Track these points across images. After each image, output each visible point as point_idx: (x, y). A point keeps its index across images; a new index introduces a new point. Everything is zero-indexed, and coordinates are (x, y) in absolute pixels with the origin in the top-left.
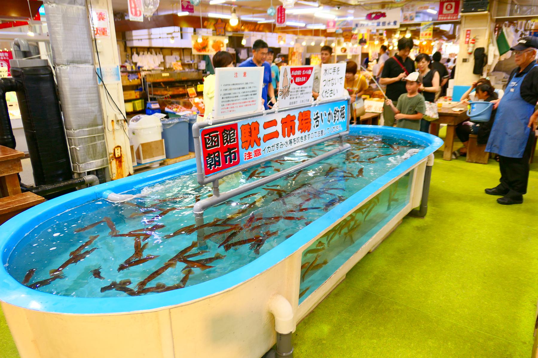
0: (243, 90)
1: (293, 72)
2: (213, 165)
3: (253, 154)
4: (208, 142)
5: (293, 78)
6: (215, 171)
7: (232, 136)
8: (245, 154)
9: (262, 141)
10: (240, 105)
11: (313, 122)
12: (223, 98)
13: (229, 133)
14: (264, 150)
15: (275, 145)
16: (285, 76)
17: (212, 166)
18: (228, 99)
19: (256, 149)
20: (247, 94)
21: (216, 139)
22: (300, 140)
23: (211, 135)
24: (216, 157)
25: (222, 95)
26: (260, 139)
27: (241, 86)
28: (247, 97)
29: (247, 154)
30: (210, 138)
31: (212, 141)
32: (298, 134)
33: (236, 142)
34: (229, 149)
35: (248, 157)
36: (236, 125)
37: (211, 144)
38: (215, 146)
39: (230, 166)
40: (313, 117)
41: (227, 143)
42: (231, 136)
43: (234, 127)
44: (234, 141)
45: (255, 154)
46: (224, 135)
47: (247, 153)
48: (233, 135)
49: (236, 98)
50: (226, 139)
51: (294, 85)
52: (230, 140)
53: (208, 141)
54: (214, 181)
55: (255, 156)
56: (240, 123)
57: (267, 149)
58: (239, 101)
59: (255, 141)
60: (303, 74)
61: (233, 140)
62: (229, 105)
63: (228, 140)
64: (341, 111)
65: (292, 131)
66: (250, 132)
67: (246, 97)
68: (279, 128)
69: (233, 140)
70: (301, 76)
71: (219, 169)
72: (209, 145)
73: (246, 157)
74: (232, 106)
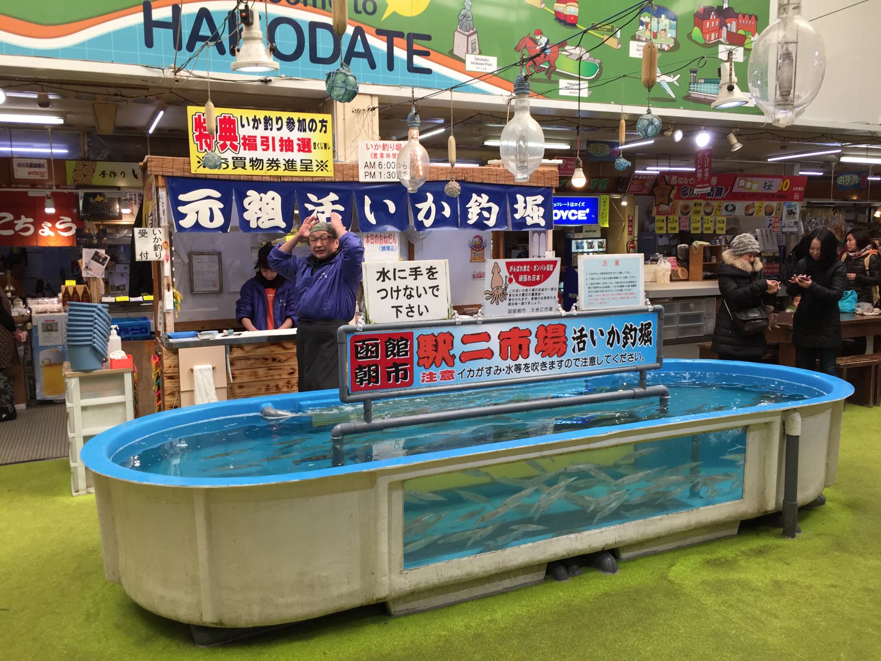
0: (616, 280)
1: (511, 268)
2: (365, 380)
3: (439, 377)
4: (361, 350)
5: (512, 276)
6: (367, 388)
7: (402, 348)
8: (424, 374)
9: (457, 360)
10: (614, 297)
11: (572, 343)
12: (589, 288)
13: (398, 343)
14: (461, 373)
15: (484, 369)
16: (496, 273)
17: (364, 382)
18: (596, 289)
19: (445, 370)
20: (622, 284)
21: (374, 348)
22: (539, 368)
23: (366, 343)
24: (372, 371)
25: (588, 284)
26: (454, 357)
27: (613, 276)
28: (622, 288)
29: (427, 375)
30: (365, 346)
31: (367, 350)
32: (534, 358)
33: (409, 356)
34: (396, 365)
35: (427, 378)
36: (412, 334)
37: (364, 353)
38: (374, 357)
39: (394, 386)
40: (570, 334)
41: (392, 356)
42: (401, 347)
43: (408, 337)
44: (406, 354)
45: (442, 376)
46: (389, 345)
47: (427, 373)
48: (404, 346)
49: (607, 289)
50: (392, 351)
51: (514, 286)
52: (399, 352)
53: (361, 350)
54: (364, 401)
55: (441, 380)
56: (417, 333)
57: (466, 373)
58: (611, 293)
59: (443, 359)
60: (535, 270)
61: (404, 353)
62: (598, 295)
63: (395, 351)
64: (641, 330)
65: (522, 350)
66: (436, 346)
67: (620, 288)
68: (494, 344)
69: (404, 353)
70: (531, 273)
71: (374, 388)
72: (362, 355)
73: (425, 378)
74: (603, 297)
